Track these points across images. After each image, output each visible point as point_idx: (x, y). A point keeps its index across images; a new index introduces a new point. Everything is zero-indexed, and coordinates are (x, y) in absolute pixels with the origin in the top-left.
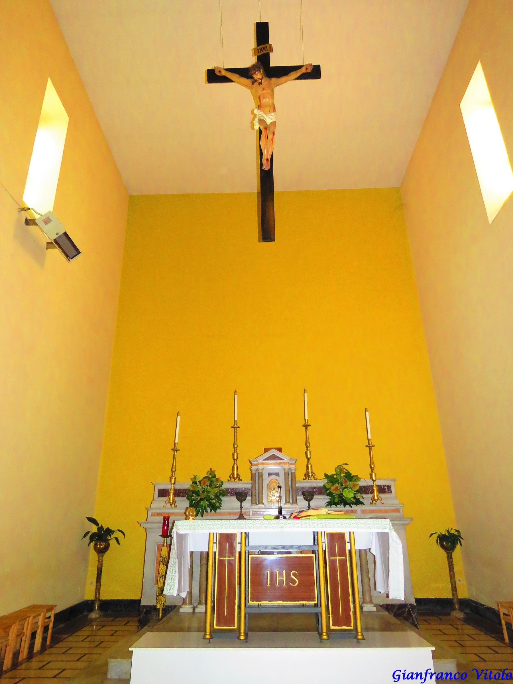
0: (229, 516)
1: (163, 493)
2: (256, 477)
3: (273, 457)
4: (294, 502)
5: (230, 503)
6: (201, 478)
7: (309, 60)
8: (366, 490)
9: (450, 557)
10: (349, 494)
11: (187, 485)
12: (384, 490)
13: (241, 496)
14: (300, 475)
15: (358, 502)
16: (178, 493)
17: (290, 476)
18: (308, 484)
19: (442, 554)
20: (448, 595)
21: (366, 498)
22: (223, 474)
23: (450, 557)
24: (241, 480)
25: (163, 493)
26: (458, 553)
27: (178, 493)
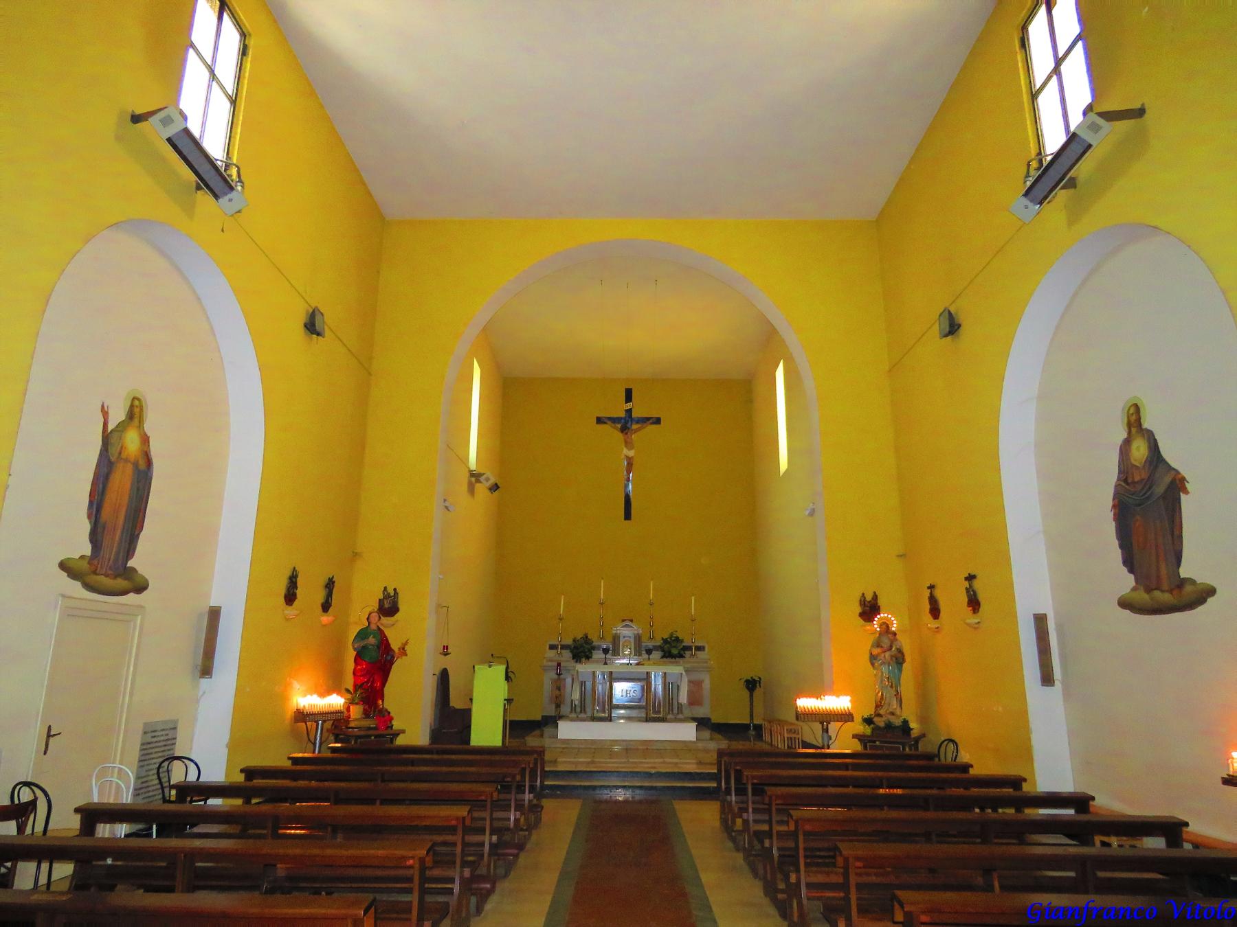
0: (597, 661)
1: (552, 647)
2: (616, 639)
3: (627, 626)
4: (640, 655)
5: (598, 655)
6: (1130, 580)
7: (655, 415)
8: (689, 648)
9: (751, 696)
10: (675, 651)
11: (569, 641)
12: (699, 648)
13: (606, 651)
14: (644, 639)
15: (681, 656)
16: (563, 647)
17: (638, 638)
18: (650, 644)
19: (746, 693)
20: (747, 721)
21: (688, 653)
22: (593, 637)
23: (751, 696)
24: (1194, 597)
25: (552, 647)
26: (758, 692)
27: (563, 647)
